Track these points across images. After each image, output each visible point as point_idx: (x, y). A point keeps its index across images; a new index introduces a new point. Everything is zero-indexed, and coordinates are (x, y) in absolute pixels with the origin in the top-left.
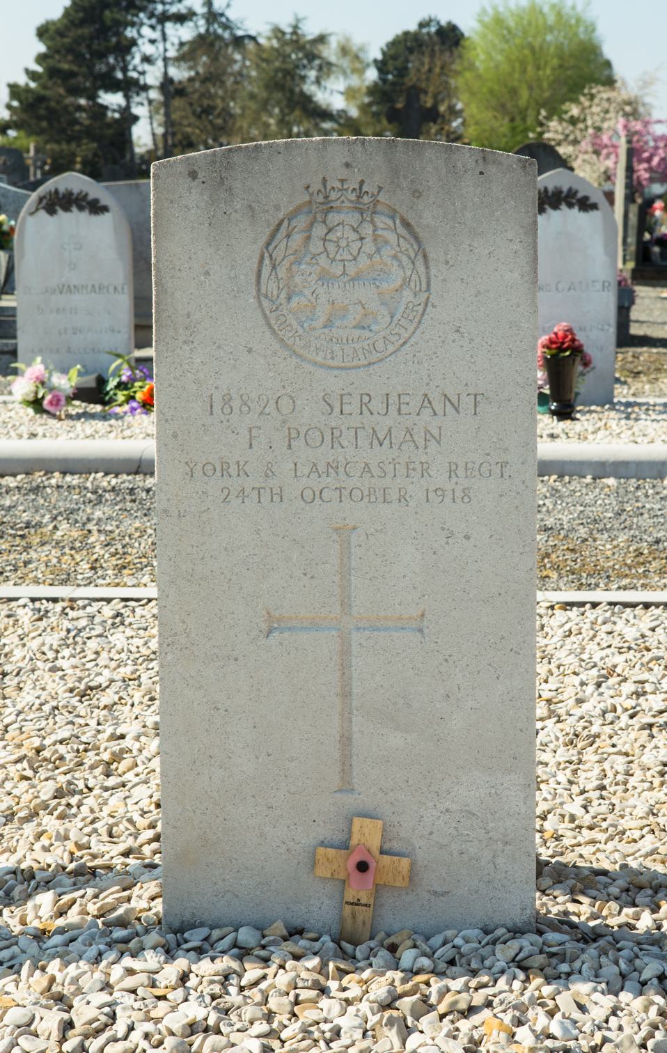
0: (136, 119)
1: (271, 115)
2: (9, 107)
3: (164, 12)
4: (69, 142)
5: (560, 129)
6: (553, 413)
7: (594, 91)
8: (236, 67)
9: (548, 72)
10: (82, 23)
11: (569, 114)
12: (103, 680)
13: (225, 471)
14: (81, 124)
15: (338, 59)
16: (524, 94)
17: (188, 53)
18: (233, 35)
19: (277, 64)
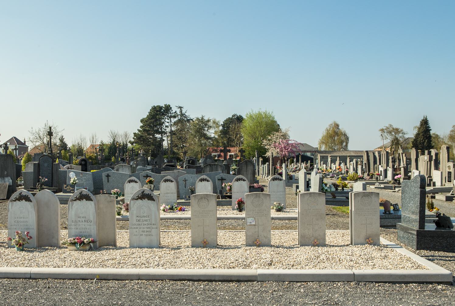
0: (164, 140)
1: (196, 138)
2: (134, 138)
4: (148, 146)
5: (266, 142)
6: (239, 211)
10: (151, 119)
12: (182, 237)
15: (213, 124)
16: (258, 133)
17: (175, 124)
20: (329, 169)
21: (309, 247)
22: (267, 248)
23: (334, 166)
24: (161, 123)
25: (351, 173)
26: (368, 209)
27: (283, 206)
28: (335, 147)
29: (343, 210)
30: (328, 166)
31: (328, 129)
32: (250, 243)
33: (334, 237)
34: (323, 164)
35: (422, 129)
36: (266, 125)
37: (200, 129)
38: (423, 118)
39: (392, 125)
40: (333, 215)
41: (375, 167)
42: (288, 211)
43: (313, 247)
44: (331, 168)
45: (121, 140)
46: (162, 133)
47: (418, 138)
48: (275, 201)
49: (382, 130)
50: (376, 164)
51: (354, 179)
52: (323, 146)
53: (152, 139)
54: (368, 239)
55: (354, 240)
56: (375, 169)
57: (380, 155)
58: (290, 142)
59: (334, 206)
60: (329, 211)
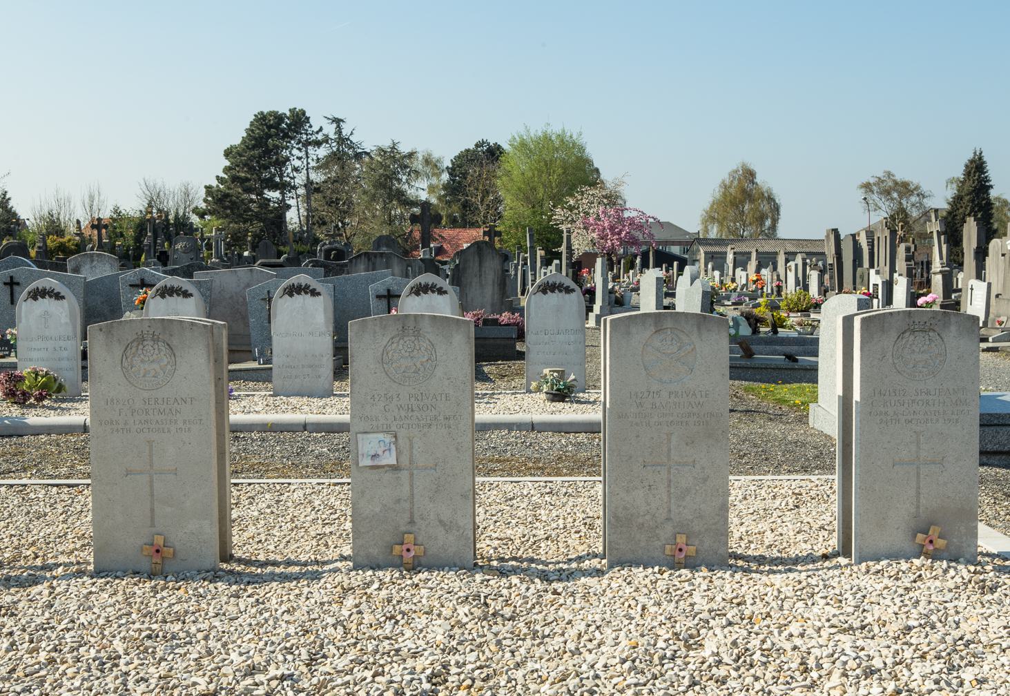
0: (289, 207)
2: (205, 201)
3: (307, 140)
4: (244, 223)
8: (357, 172)
10: (254, 147)
13: (112, 423)
14: (253, 211)
17: (324, 165)
19: (381, 171)
20: (728, 282)
21: (650, 570)
22: (452, 580)
23: (744, 273)
24: (281, 159)
25: (788, 292)
26: (928, 393)
27: (574, 380)
28: (744, 231)
29: (778, 396)
30: (727, 275)
31: (727, 182)
32: (374, 551)
33: (761, 512)
34: (713, 270)
35: (968, 184)
37: (387, 177)
38: (971, 156)
39: (893, 172)
40: (747, 411)
41: (858, 276)
42: (591, 400)
43: (666, 575)
44: (733, 280)
45: (172, 205)
46: (284, 187)
47: (958, 209)
48: (547, 365)
49: (867, 187)
50: (861, 265)
51: (800, 308)
53: (255, 202)
54: (926, 532)
55: (860, 535)
56: (858, 280)
57: (873, 240)
58: (626, 214)
59: (747, 383)
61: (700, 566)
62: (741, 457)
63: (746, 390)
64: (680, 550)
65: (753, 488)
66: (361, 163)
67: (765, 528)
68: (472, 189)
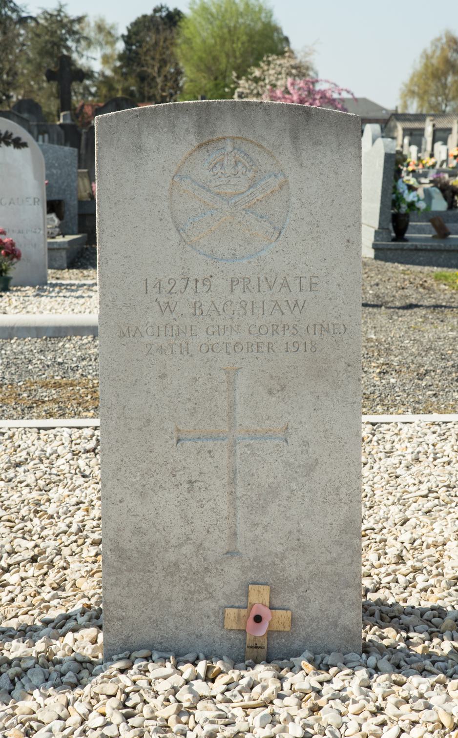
5: (247, 85)
7: (270, 59)
9: (240, 45)
11: (253, 75)
15: (96, 34)
16: (223, 60)
18: (19, 16)
19: (47, 37)
28: (446, 106)
30: (425, 150)
31: (429, 52)
33: (442, 493)
34: (410, 144)
36: (247, 34)
37: (54, 44)
40: (436, 307)
44: (432, 156)
52: (412, 103)
58: (318, 87)
59: (440, 269)
60: (421, 290)
61: (298, 654)
62: (421, 377)
63: (438, 278)
64: (258, 619)
65: (432, 438)
66: (25, 27)
67: (446, 535)
68: (148, 58)
